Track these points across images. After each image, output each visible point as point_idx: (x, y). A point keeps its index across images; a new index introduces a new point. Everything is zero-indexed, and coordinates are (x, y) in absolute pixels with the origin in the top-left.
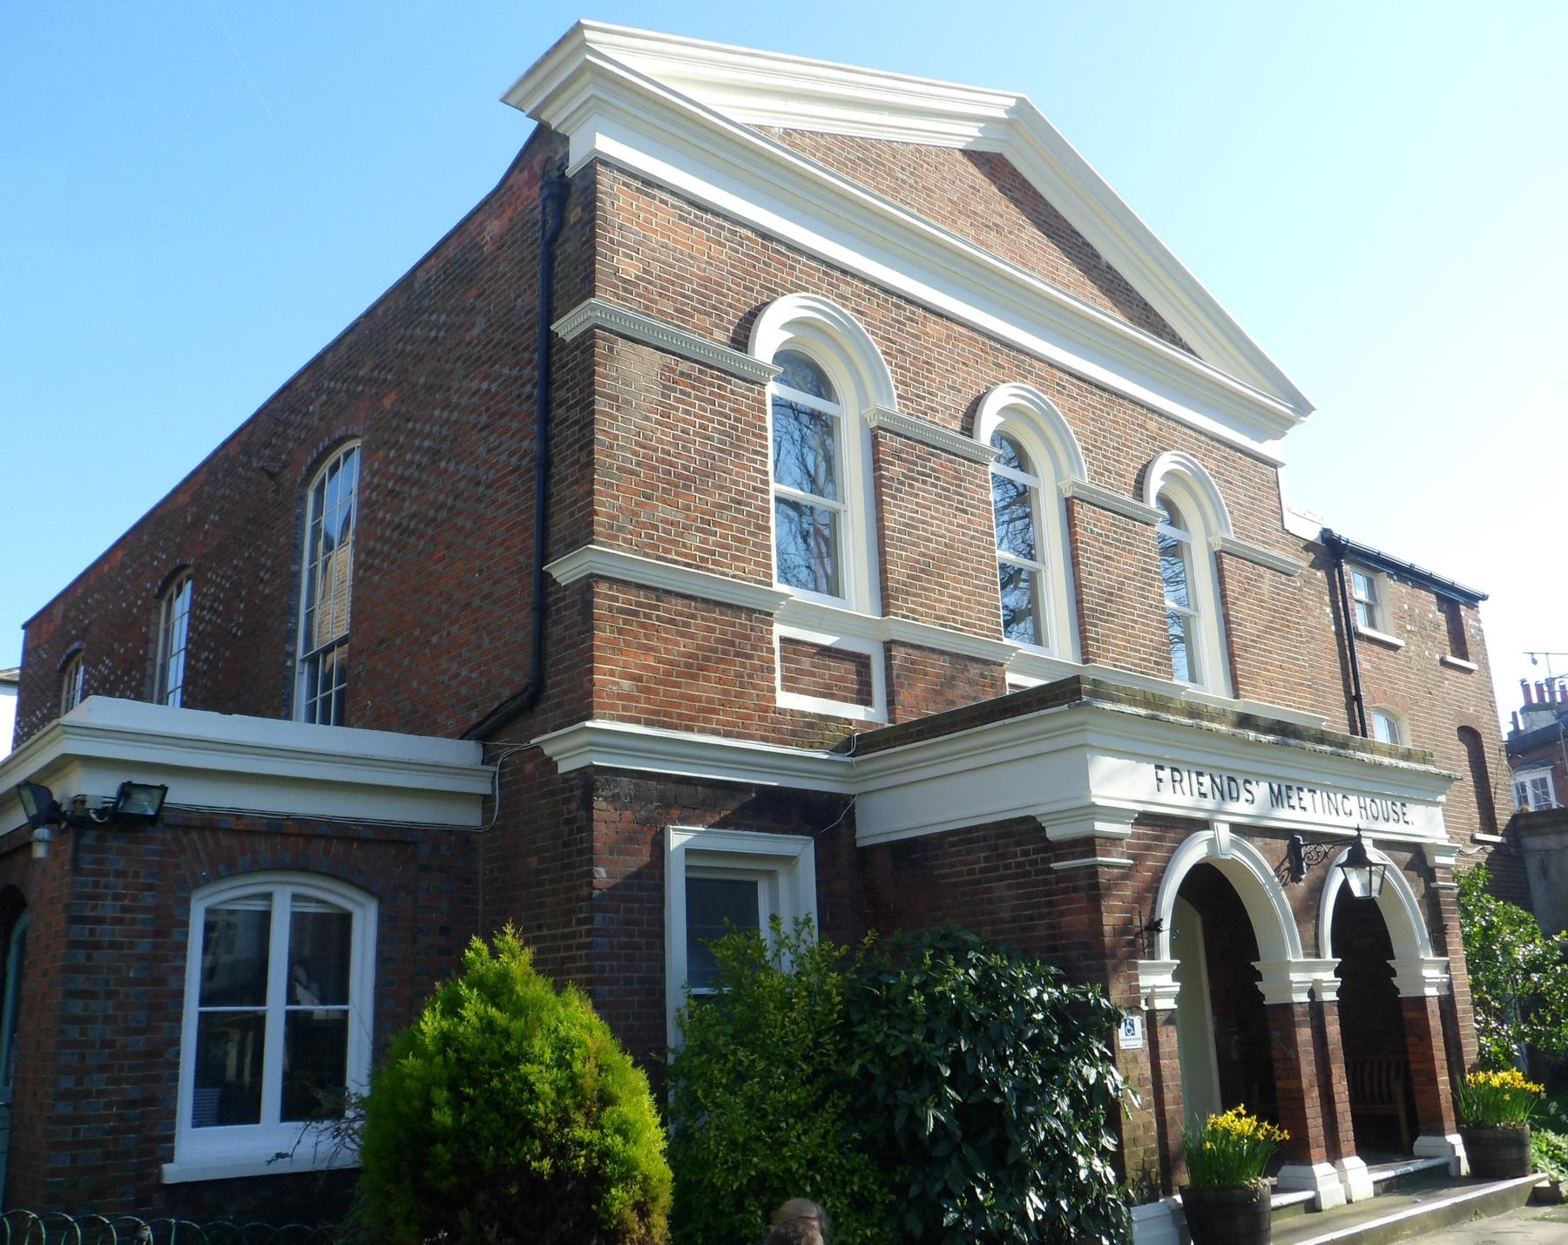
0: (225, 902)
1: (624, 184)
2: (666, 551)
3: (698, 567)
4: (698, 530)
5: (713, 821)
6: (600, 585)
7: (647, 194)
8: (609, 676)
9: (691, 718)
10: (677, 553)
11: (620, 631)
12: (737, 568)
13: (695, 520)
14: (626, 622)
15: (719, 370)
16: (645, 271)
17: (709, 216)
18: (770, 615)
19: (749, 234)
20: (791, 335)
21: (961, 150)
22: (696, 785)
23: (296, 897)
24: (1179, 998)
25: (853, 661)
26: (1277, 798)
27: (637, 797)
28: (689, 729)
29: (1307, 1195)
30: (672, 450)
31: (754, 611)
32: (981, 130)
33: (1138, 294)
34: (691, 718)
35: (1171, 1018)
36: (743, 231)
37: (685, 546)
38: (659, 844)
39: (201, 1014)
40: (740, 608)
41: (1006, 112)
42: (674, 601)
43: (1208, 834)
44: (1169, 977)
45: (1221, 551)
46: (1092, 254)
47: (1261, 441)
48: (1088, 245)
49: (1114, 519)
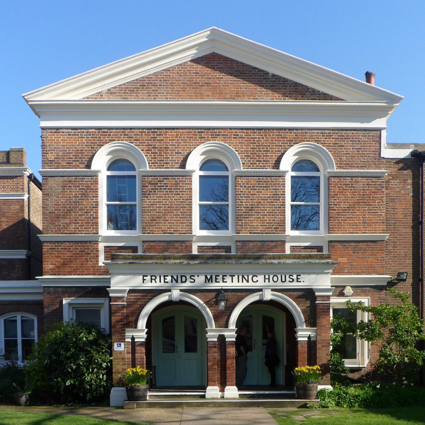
0: (8, 318)
1: (51, 132)
2: (63, 231)
3: (73, 234)
4: (73, 223)
5: (77, 296)
6: (44, 243)
7: (57, 132)
8: (47, 266)
9: (71, 272)
10: (67, 231)
11: (50, 254)
12: (86, 231)
13: (73, 221)
14: (52, 251)
15: (81, 176)
16: (57, 156)
17: (79, 131)
18: (98, 241)
19: (94, 130)
20: (112, 156)
21: (190, 61)
22: (72, 288)
23: (22, 317)
24: (146, 339)
25: (131, 249)
26: (208, 280)
27: (56, 292)
28: (70, 275)
29: (203, 393)
30: (65, 204)
31: (92, 241)
32: (197, 50)
33: (291, 81)
34: (71, 272)
35: (141, 344)
36: (91, 130)
37: (69, 228)
38: (61, 302)
39: (22, 340)
40: (87, 242)
41: (207, 38)
42: (66, 243)
43: (169, 293)
44: (235, 332)
45: (330, 177)
46: (264, 74)
47: (369, 122)
48: (262, 71)
49: (259, 179)
